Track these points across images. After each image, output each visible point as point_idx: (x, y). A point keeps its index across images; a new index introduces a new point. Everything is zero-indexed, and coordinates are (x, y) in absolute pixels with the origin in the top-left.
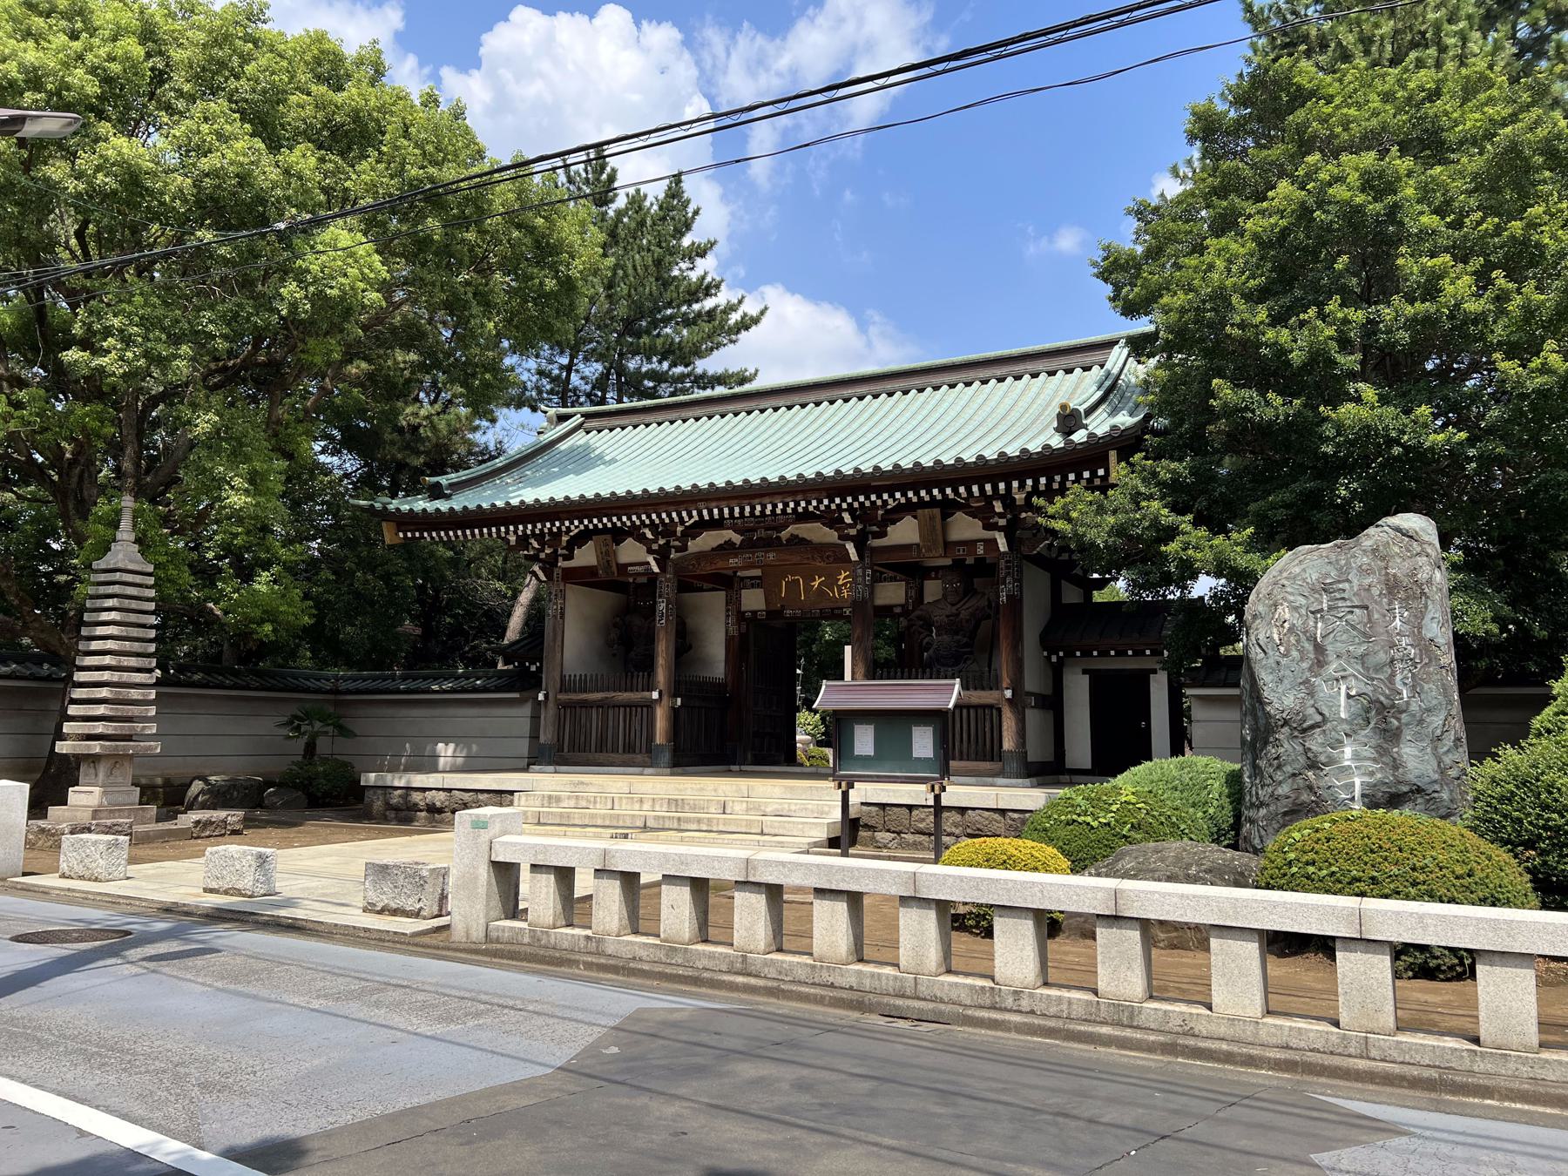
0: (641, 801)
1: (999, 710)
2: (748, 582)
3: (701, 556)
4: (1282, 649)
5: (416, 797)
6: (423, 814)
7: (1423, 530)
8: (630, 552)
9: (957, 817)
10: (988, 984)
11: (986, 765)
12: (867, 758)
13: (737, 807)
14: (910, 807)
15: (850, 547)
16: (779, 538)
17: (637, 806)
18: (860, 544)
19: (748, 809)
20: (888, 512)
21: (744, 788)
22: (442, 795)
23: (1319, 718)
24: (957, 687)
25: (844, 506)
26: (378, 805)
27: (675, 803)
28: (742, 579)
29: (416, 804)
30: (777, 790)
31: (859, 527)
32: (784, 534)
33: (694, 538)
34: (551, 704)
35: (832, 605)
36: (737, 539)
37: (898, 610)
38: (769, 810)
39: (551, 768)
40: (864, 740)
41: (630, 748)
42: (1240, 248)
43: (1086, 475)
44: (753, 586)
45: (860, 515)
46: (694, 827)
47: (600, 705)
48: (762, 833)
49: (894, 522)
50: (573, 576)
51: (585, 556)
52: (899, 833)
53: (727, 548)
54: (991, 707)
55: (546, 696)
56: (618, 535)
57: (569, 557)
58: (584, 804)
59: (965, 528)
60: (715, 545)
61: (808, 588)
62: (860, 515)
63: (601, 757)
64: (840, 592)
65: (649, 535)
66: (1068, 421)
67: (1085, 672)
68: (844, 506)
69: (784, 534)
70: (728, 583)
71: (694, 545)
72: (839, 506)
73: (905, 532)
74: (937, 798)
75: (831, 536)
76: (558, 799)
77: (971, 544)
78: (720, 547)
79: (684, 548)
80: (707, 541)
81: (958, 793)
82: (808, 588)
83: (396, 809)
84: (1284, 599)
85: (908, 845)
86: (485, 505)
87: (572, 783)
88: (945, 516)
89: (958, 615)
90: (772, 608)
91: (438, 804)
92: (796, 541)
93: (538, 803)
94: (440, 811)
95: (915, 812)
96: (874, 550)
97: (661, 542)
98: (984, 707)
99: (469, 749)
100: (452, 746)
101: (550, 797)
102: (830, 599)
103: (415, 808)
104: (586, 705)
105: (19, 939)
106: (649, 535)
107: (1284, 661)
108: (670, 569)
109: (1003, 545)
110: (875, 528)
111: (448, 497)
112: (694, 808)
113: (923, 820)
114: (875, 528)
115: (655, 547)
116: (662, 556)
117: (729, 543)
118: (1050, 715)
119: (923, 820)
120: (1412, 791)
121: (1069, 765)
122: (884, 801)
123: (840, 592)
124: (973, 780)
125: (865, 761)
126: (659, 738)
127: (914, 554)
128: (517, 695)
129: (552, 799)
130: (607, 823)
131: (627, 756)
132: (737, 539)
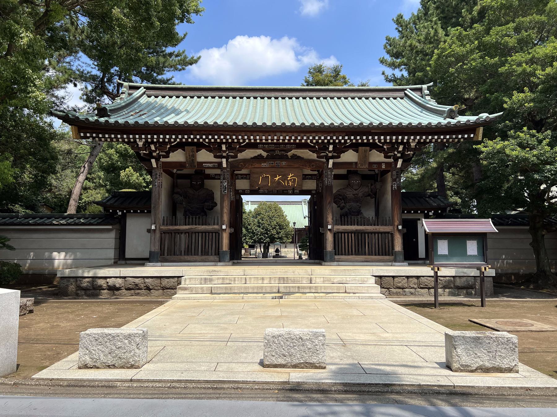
0: (263, 279)
2: (240, 176)
5: (101, 282)
6: (106, 291)
9: (415, 280)
11: (387, 257)
12: (474, 256)
13: (318, 280)
14: (393, 277)
16: (287, 155)
17: (260, 282)
19: (324, 281)
21: (309, 271)
22: (120, 281)
25: (331, 141)
26: (72, 288)
27: (282, 280)
28: (237, 175)
29: (101, 286)
30: (327, 271)
31: (157, 152)
32: (290, 154)
34: (157, 231)
35: (284, 189)
36: (264, 154)
37: (314, 192)
38: (335, 281)
39: (159, 264)
40: (443, 247)
42: (61, 53)
43: (418, 137)
44: (242, 178)
46: (308, 291)
47: (186, 232)
48: (346, 292)
52: (388, 289)
54: (388, 233)
56: (199, 146)
58: (228, 282)
60: (252, 156)
62: (230, 146)
64: (288, 183)
68: (331, 141)
69: (290, 154)
71: (241, 156)
72: (329, 141)
76: (211, 280)
77: (380, 164)
78: (255, 158)
80: (249, 154)
83: (85, 289)
85: (393, 293)
86: (120, 121)
87: (208, 271)
89: (358, 194)
90: (253, 189)
91: (118, 286)
92: (295, 157)
93: (277, 282)
94: (118, 289)
95: (396, 279)
98: (385, 233)
99: (76, 255)
100: (63, 255)
101: (205, 279)
102: (282, 186)
103: (100, 288)
104: (179, 232)
111: (109, 116)
112: (294, 282)
114: (164, 154)
117: (260, 156)
119: (400, 282)
121: (127, 256)
122: (382, 275)
123: (288, 183)
124: (382, 264)
125: (443, 257)
127: (354, 166)
128: (110, 227)
130: (255, 291)
131: (204, 257)
132: (264, 154)
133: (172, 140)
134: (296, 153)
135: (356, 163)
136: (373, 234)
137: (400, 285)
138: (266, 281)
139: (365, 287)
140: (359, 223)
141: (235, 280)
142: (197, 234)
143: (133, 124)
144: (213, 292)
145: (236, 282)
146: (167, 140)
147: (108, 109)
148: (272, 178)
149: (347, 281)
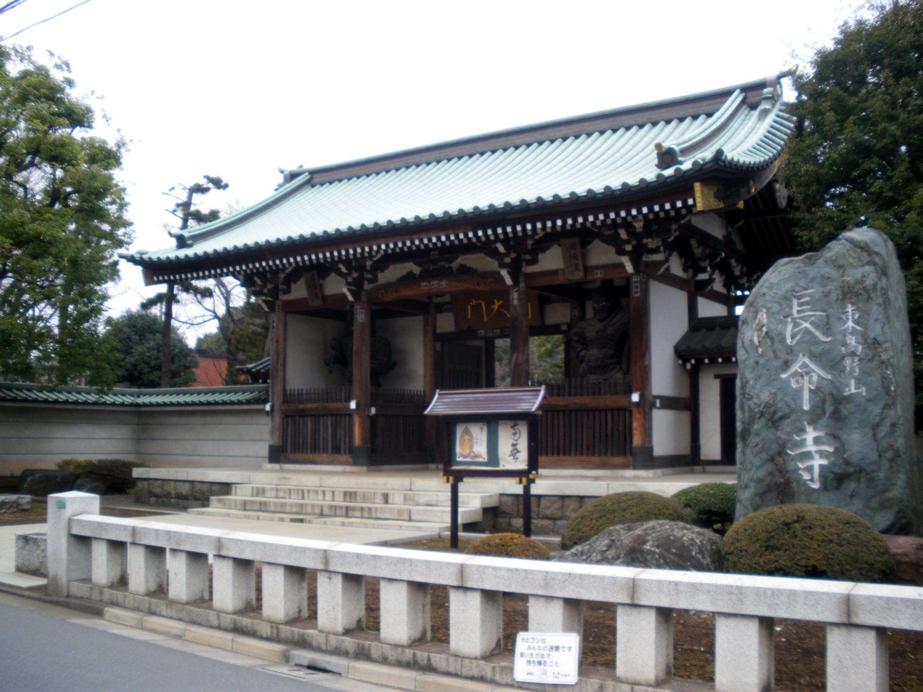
1: (630, 411)
3: (387, 286)
4: (760, 350)
7: (872, 241)
8: (336, 286)
10: (40, 582)
15: (504, 273)
16: (450, 268)
18: (515, 273)
20: (537, 242)
23: (786, 410)
24: (542, 393)
27: (349, 495)
31: (513, 255)
32: (455, 265)
33: (382, 270)
36: (416, 270)
37: (564, 328)
41: (336, 450)
45: (514, 243)
49: (543, 250)
50: (293, 308)
51: (299, 291)
53: (409, 278)
55: (272, 407)
57: (288, 291)
59: (601, 255)
61: (489, 310)
63: (297, 456)
65: (344, 270)
66: (666, 157)
67: (716, 376)
69: (455, 265)
70: (423, 307)
71: (385, 277)
73: (551, 260)
74: (527, 489)
75: (491, 264)
79: (375, 279)
81: (547, 483)
82: (489, 310)
84: (764, 306)
88: (585, 244)
92: (465, 270)
96: (529, 276)
97: (355, 275)
105: (340, 674)
106: (344, 270)
107: (762, 361)
108: (364, 298)
109: (629, 268)
110: (528, 257)
111: (190, 246)
113: (548, 508)
114: (528, 257)
115: (350, 279)
116: (357, 287)
117: (411, 274)
118: (686, 416)
119: (548, 508)
120: (856, 472)
122: (582, 493)
126: (357, 441)
129: (260, 492)
132: (416, 270)
133: (374, 253)
134: (465, 262)
135: (563, 270)
136: (343, 417)
137: (548, 512)
138: (329, 496)
139: (438, 511)
140: (573, 390)
141: (290, 493)
142: (603, 414)
143: (601, 193)
144: (413, 518)
145: (292, 496)
146: (366, 255)
147: (677, 149)
148: (488, 307)
149: (437, 501)
